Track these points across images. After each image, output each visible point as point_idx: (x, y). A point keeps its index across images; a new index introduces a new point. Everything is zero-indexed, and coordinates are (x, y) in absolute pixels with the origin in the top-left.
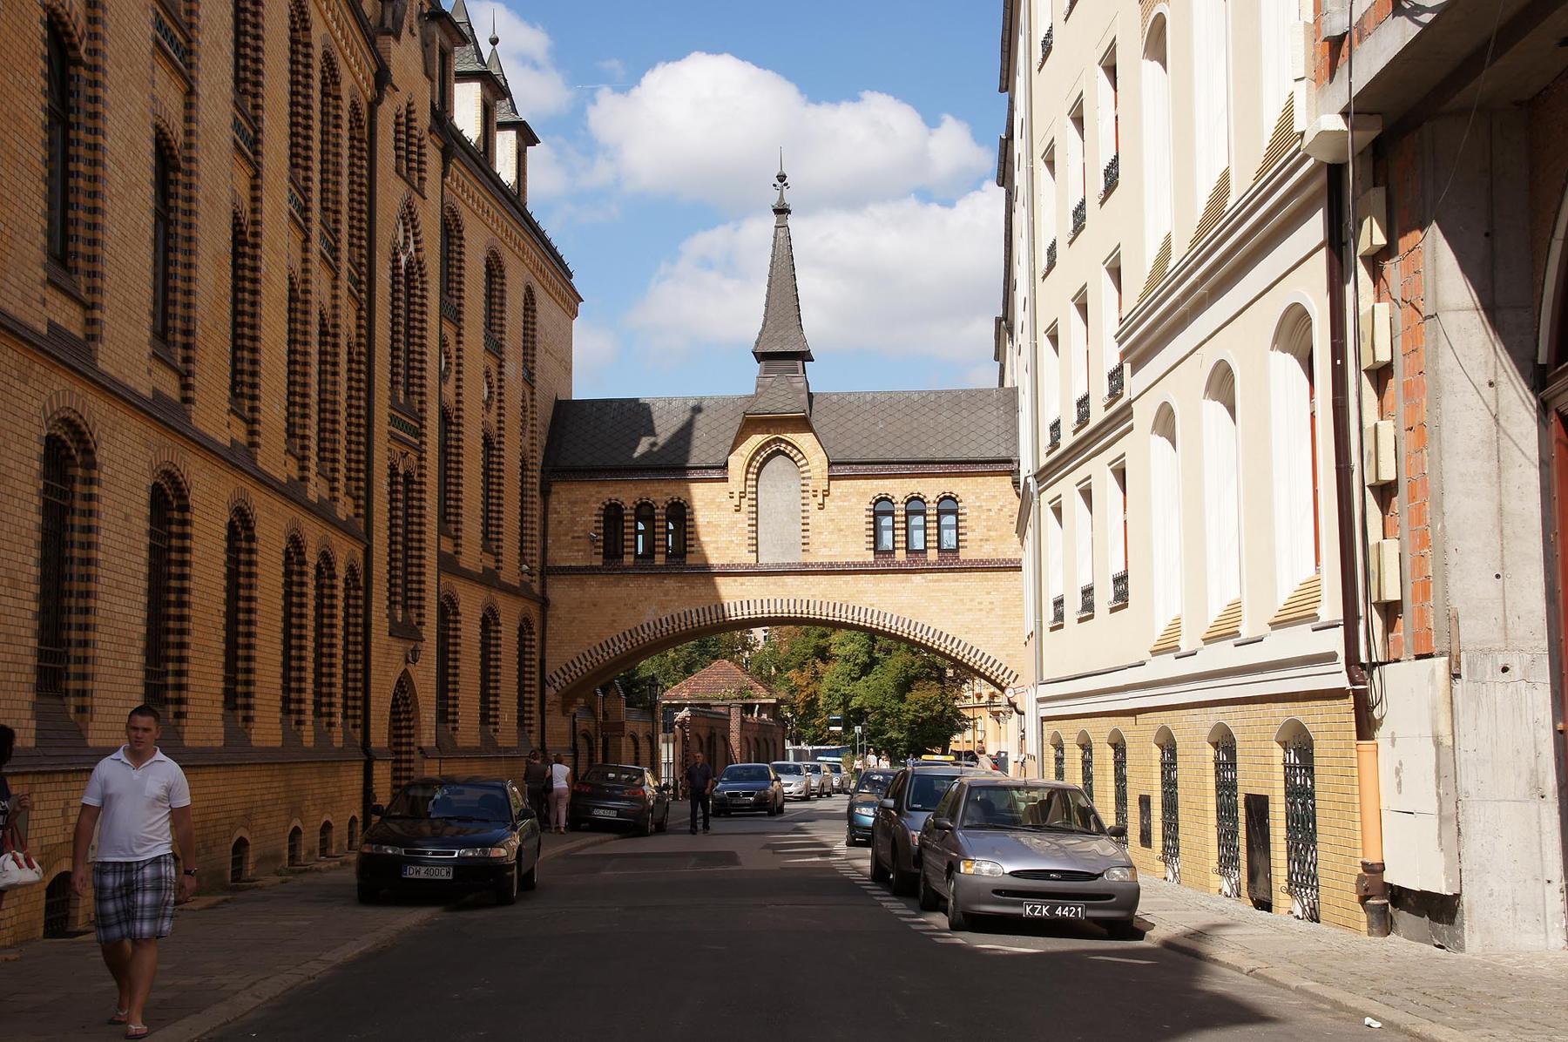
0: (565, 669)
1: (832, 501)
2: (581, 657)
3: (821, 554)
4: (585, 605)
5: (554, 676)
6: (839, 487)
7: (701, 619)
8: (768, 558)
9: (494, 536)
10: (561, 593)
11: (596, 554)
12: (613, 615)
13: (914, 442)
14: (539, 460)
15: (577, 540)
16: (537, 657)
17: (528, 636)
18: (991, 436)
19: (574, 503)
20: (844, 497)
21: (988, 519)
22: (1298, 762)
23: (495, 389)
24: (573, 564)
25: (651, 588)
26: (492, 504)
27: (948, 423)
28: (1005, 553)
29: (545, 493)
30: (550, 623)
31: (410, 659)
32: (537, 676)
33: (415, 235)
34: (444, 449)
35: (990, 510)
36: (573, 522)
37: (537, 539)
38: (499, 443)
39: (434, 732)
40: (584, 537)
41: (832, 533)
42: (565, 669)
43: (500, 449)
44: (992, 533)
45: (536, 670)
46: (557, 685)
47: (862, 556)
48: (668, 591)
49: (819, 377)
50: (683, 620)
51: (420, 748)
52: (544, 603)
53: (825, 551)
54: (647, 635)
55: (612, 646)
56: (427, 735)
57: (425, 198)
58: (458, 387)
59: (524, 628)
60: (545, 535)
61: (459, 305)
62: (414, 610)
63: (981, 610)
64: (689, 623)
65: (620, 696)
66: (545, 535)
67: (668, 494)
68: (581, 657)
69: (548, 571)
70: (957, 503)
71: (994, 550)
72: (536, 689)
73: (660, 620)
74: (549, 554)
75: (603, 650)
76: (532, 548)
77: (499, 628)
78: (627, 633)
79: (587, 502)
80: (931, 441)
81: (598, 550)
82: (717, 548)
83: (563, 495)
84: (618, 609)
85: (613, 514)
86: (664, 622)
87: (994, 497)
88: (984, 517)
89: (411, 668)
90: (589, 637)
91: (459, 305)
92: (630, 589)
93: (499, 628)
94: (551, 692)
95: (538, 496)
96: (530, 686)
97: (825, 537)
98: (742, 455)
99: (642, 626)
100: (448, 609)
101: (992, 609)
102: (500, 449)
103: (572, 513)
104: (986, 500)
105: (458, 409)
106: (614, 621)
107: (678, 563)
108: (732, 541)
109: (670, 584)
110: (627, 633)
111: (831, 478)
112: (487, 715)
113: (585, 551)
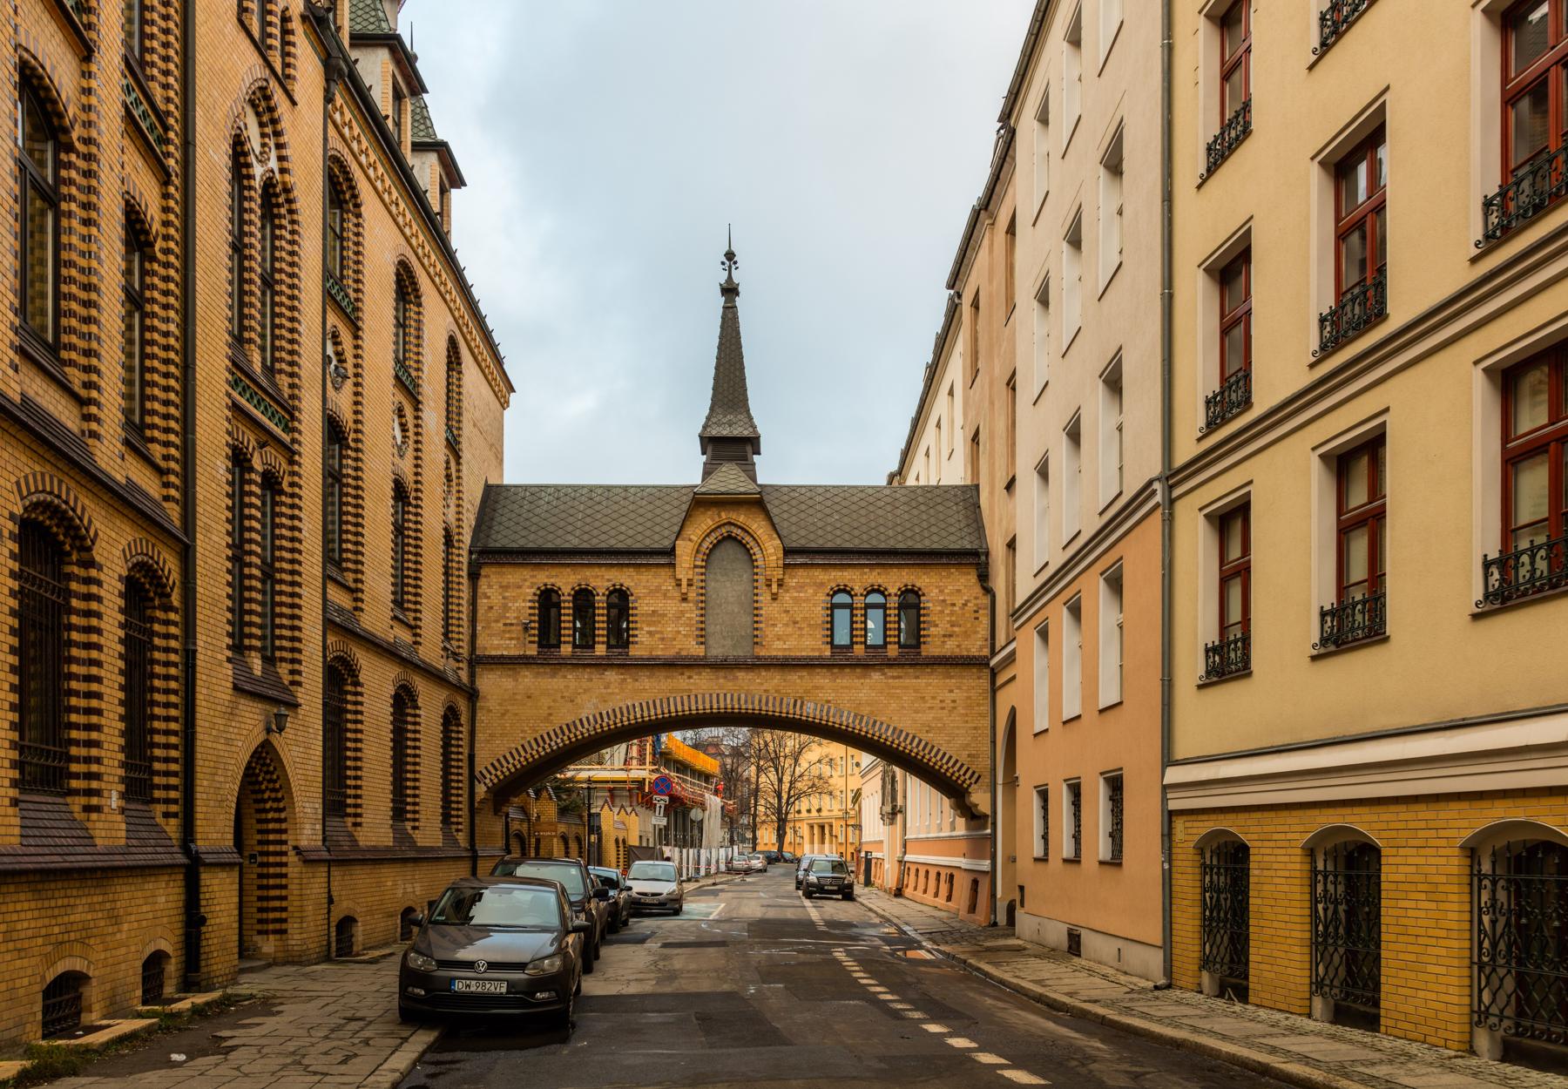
0: (497, 764)
1: (787, 591)
2: (514, 752)
3: (778, 644)
4: (518, 697)
5: (484, 772)
6: (796, 578)
7: (646, 714)
8: (717, 650)
9: (411, 606)
10: (491, 684)
11: (530, 642)
12: (549, 708)
13: (873, 533)
14: (467, 538)
15: (508, 628)
16: (466, 751)
17: (454, 728)
18: (952, 530)
19: (505, 588)
20: (800, 587)
21: (952, 613)
22: (1215, 862)
23: (411, 434)
24: (505, 653)
25: (591, 680)
26: (408, 569)
27: (906, 516)
28: (968, 650)
29: (474, 577)
30: (480, 715)
31: (274, 727)
32: (465, 771)
33: (279, 146)
34: (333, 478)
35: (954, 605)
36: (505, 608)
37: (465, 623)
38: (417, 498)
39: (319, 827)
40: (517, 625)
41: (786, 625)
42: (497, 764)
43: (417, 506)
44: (956, 629)
45: (465, 764)
46: (487, 781)
47: (819, 649)
48: (610, 683)
49: (771, 469)
50: (626, 714)
51: (295, 848)
52: (472, 695)
53: (778, 644)
54: (585, 731)
55: (548, 741)
56: (307, 826)
57: (294, 103)
58: (357, 394)
59: (450, 717)
60: (473, 621)
61: (357, 300)
62: (284, 664)
63: (943, 708)
64: (632, 717)
65: (551, 798)
66: (473, 621)
67: (609, 580)
68: (514, 752)
69: (478, 662)
70: (919, 596)
71: (958, 646)
72: (465, 785)
73: (601, 714)
74: (478, 642)
75: (538, 745)
76: (459, 633)
77: (418, 712)
78: (565, 727)
79: (520, 587)
80: (891, 533)
81: (532, 639)
82: (663, 639)
83: (494, 579)
84: (554, 701)
85: (547, 599)
86: (605, 716)
87: (959, 591)
88: (947, 612)
89: (276, 740)
90: (523, 731)
91: (357, 300)
92: (569, 681)
93: (418, 712)
94: (481, 790)
95: (466, 577)
96: (458, 802)
97: (779, 629)
98: (690, 540)
99: (581, 720)
100: (339, 676)
101: (955, 708)
102: (417, 506)
103: (504, 598)
104: (951, 594)
105: (357, 431)
106: (550, 714)
107: (620, 654)
108: (679, 632)
109: (612, 676)
110: (565, 727)
111: (786, 566)
112: (401, 809)
113: (518, 639)
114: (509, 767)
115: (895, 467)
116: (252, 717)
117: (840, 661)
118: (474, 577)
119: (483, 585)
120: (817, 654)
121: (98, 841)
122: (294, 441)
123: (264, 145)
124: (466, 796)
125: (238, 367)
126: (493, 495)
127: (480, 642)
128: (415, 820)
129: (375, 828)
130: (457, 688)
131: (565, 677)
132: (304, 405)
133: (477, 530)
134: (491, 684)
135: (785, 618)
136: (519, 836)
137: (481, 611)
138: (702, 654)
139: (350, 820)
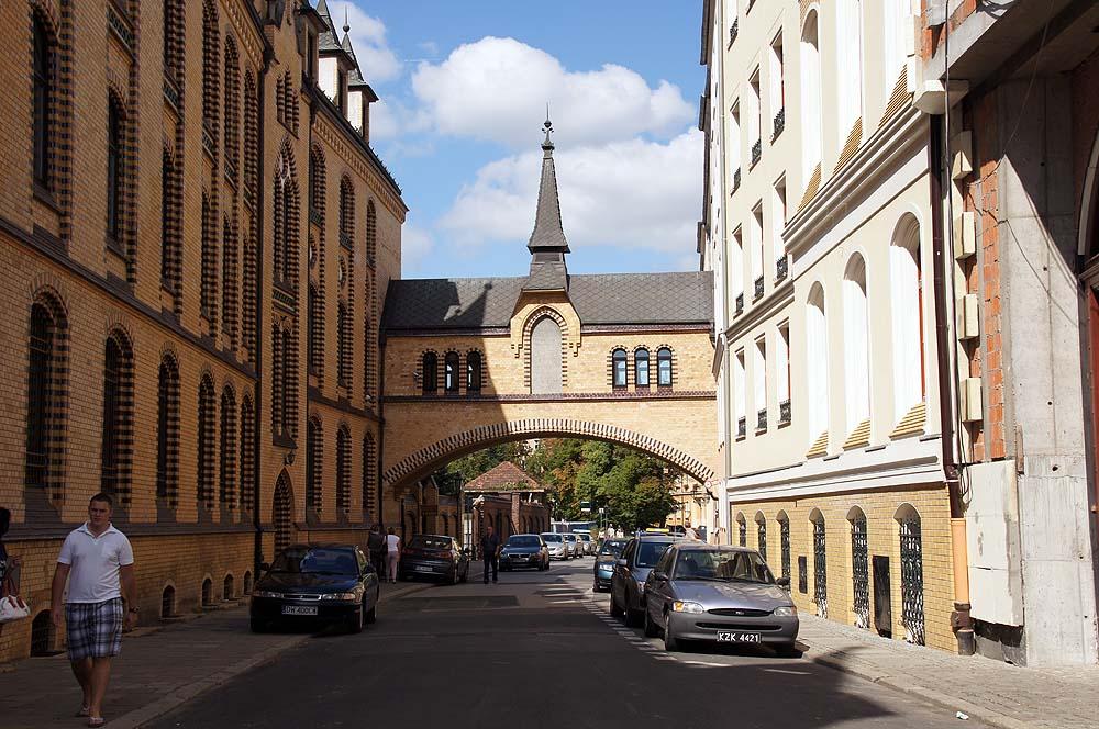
8: (538, 391)
10: (392, 414)
19: (403, 352)
20: (592, 348)
29: (382, 345)
32: (376, 473)
36: (403, 366)
38: (350, 310)
49: (575, 264)
52: (382, 422)
54: (453, 445)
69: (384, 400)
85: (429, 360)
87: (697, 348)
88: (690, 362)
89: (288, 467)
91: (322, 213)
94: (386, 484)
109: (470, 409)
111: (582, 335)
112: (341, 501)
114: (404, 470)
115: (701, 220)
116: (280, 453)
117: (618, 394)
118: (382, 345)
119: (388, 351)
120: (603, 392)
121: (131, 520)
122: (296, 310)
123: (285, 166)
124: (377, 489)
125: (276, 278)
126: (398, 289)
127: (387, 388)
128: (347, 506)
129: (187, 510)
130: (372, 418)
131: (440, 410)
132: (300, 290)
133: (384, 315)
134: (392, 414)
135: (583, 368)
136: (411, 515)
137: (387, 367)
138: (927, 82)
139: (345, 509)
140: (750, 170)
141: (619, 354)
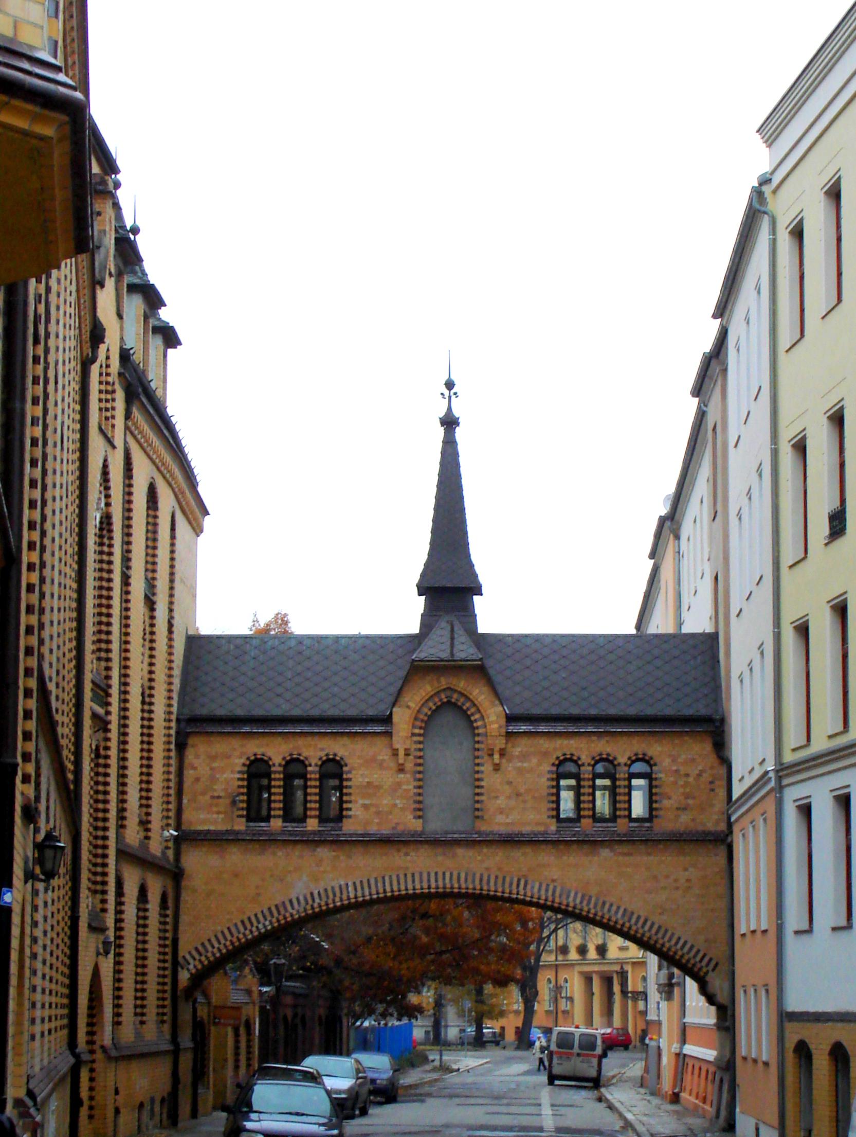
19: (213, 758)
20: (524, 757)
29: (181, 747)
52: (177, 875)
88: (681, 783)
111: (509, 735)
118: (181, 747)
126: (196, 643)
140: (740, 509)
141: (294, 768)
